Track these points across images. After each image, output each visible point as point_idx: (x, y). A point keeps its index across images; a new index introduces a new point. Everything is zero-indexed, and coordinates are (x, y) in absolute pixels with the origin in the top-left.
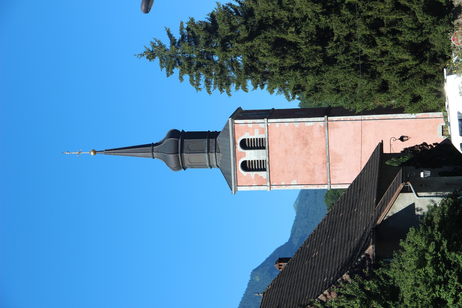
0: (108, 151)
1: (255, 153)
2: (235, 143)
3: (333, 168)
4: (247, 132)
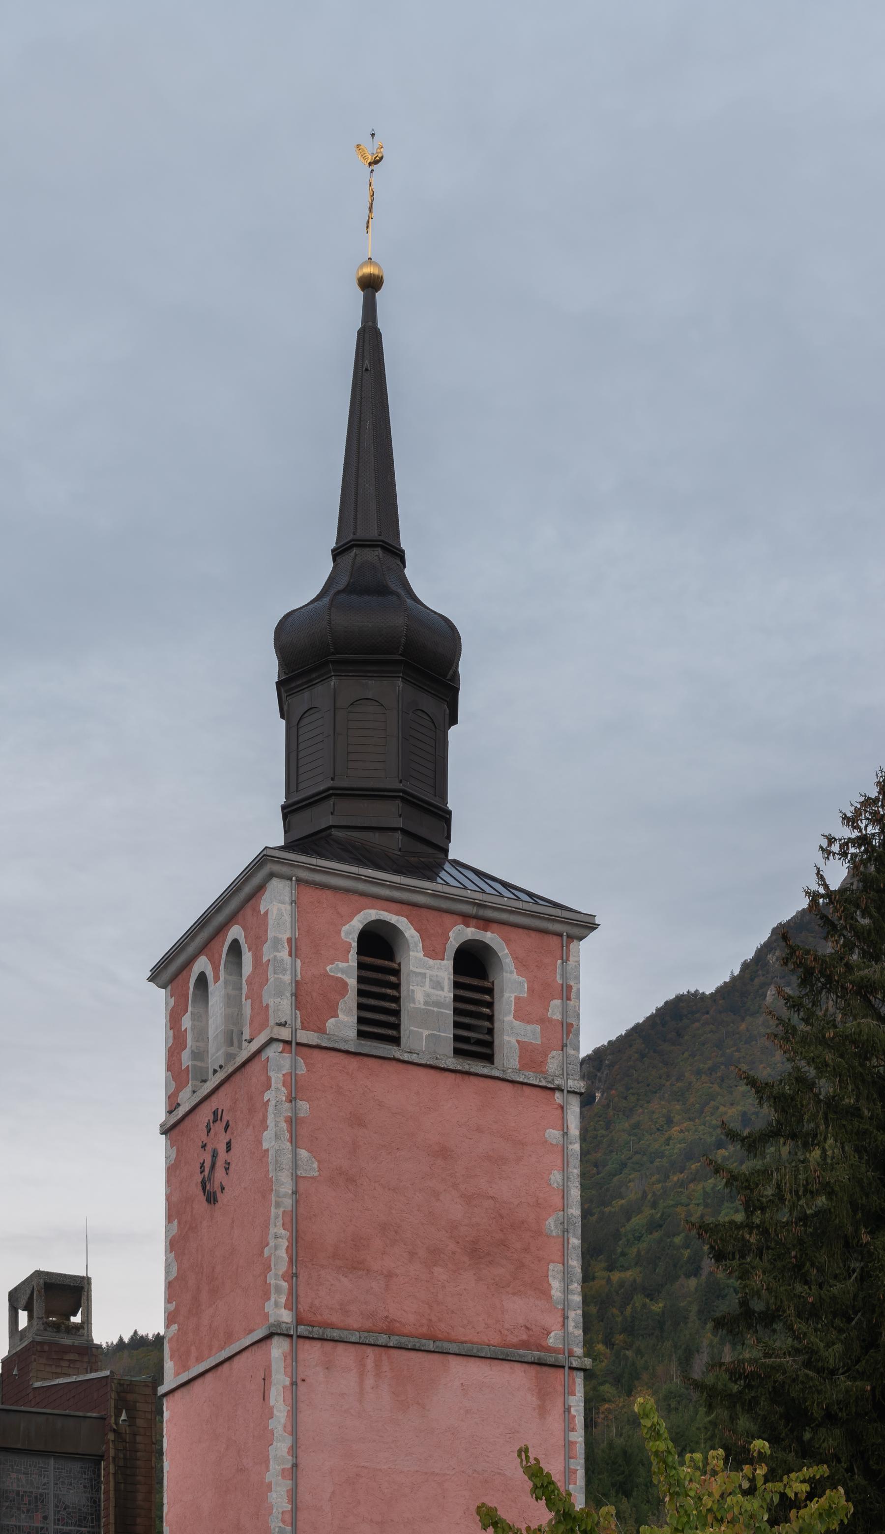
0: (370, 342)
1: (437, 1004)
3: (370, 1363)
4: (531, 990)
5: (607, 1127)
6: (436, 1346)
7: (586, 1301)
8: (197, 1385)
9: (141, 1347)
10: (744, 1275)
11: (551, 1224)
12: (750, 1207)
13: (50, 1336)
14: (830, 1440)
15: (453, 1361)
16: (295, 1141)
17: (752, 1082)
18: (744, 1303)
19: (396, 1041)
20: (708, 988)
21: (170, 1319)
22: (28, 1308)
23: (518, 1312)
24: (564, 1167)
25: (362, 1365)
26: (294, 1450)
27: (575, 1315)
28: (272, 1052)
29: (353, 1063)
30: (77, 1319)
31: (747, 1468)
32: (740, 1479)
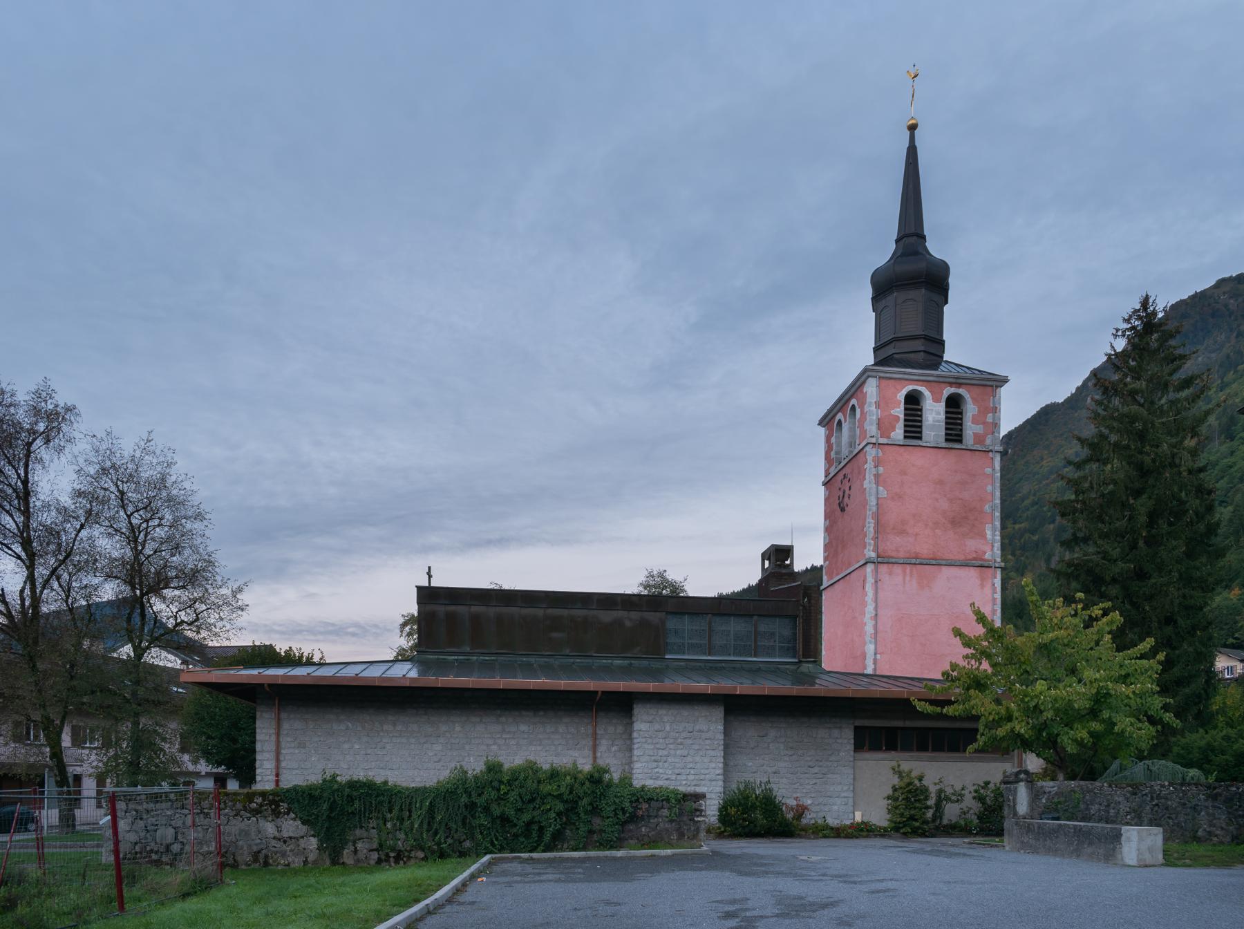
0: (912, 152)
5: (1014, 464)
6: (937, 562)
7: (1002, 538)
8: (836, 586)
9: (815, 571)
10: (1074, 522)
11: (987, 508)
12: (1077, 493)
13: (777, 570)
14: (1114, 590)
16: (877, 484)
17: (1079, 439)
18: (1074, 534)
19: (920, 438)
20: (1061, 401)
21: (826, 559)
22: (769, 559)
23: (972, 545)
24: (993, 484)
25: (904, 572)
26: (876, 609)
27: (997, 545)
28: (867, 448)
29: (902, 449)
30: (788, 562)
31: (1073, 606)
32: (1071, 610)
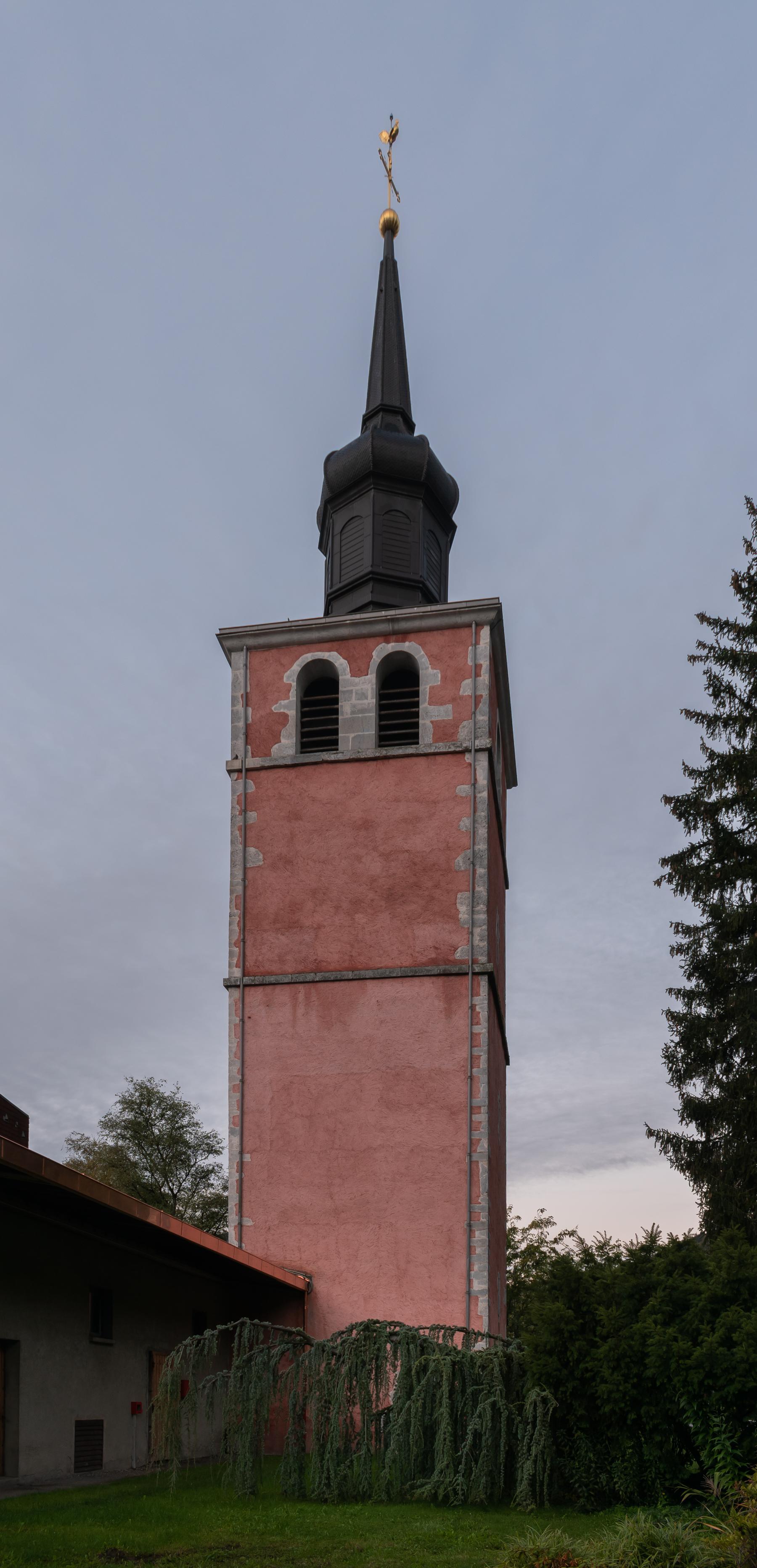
0: (389, 271)
1: (363, 711)
2: (403, 635)
3: (301, 997)
4: (444, 678)
6: (357, 975)
11: (460, 862)
15: (370, 984)
23: (427, 936)
25: (294, 998)
29: (292, 773)
